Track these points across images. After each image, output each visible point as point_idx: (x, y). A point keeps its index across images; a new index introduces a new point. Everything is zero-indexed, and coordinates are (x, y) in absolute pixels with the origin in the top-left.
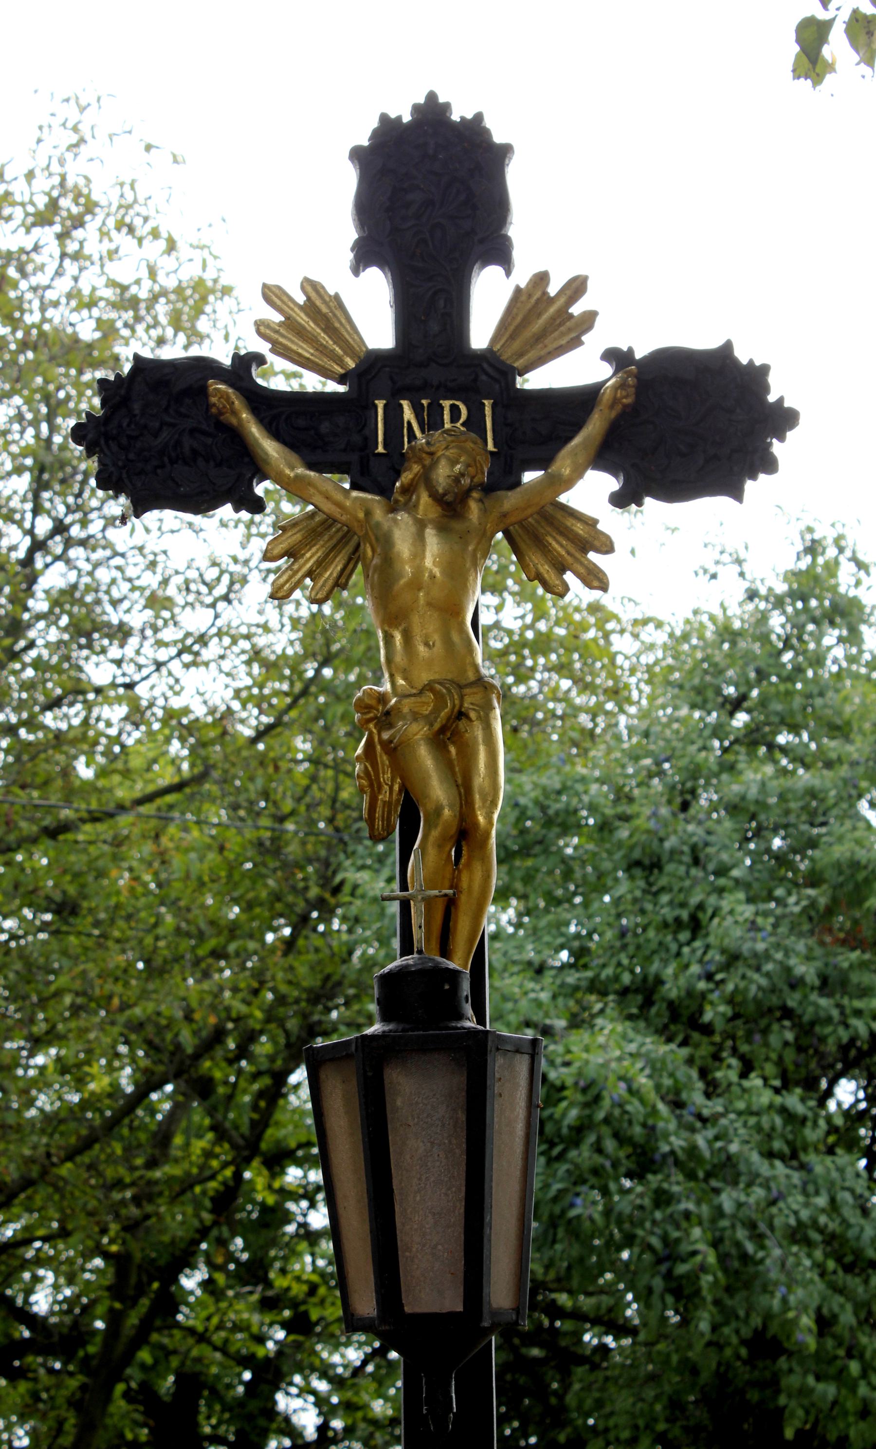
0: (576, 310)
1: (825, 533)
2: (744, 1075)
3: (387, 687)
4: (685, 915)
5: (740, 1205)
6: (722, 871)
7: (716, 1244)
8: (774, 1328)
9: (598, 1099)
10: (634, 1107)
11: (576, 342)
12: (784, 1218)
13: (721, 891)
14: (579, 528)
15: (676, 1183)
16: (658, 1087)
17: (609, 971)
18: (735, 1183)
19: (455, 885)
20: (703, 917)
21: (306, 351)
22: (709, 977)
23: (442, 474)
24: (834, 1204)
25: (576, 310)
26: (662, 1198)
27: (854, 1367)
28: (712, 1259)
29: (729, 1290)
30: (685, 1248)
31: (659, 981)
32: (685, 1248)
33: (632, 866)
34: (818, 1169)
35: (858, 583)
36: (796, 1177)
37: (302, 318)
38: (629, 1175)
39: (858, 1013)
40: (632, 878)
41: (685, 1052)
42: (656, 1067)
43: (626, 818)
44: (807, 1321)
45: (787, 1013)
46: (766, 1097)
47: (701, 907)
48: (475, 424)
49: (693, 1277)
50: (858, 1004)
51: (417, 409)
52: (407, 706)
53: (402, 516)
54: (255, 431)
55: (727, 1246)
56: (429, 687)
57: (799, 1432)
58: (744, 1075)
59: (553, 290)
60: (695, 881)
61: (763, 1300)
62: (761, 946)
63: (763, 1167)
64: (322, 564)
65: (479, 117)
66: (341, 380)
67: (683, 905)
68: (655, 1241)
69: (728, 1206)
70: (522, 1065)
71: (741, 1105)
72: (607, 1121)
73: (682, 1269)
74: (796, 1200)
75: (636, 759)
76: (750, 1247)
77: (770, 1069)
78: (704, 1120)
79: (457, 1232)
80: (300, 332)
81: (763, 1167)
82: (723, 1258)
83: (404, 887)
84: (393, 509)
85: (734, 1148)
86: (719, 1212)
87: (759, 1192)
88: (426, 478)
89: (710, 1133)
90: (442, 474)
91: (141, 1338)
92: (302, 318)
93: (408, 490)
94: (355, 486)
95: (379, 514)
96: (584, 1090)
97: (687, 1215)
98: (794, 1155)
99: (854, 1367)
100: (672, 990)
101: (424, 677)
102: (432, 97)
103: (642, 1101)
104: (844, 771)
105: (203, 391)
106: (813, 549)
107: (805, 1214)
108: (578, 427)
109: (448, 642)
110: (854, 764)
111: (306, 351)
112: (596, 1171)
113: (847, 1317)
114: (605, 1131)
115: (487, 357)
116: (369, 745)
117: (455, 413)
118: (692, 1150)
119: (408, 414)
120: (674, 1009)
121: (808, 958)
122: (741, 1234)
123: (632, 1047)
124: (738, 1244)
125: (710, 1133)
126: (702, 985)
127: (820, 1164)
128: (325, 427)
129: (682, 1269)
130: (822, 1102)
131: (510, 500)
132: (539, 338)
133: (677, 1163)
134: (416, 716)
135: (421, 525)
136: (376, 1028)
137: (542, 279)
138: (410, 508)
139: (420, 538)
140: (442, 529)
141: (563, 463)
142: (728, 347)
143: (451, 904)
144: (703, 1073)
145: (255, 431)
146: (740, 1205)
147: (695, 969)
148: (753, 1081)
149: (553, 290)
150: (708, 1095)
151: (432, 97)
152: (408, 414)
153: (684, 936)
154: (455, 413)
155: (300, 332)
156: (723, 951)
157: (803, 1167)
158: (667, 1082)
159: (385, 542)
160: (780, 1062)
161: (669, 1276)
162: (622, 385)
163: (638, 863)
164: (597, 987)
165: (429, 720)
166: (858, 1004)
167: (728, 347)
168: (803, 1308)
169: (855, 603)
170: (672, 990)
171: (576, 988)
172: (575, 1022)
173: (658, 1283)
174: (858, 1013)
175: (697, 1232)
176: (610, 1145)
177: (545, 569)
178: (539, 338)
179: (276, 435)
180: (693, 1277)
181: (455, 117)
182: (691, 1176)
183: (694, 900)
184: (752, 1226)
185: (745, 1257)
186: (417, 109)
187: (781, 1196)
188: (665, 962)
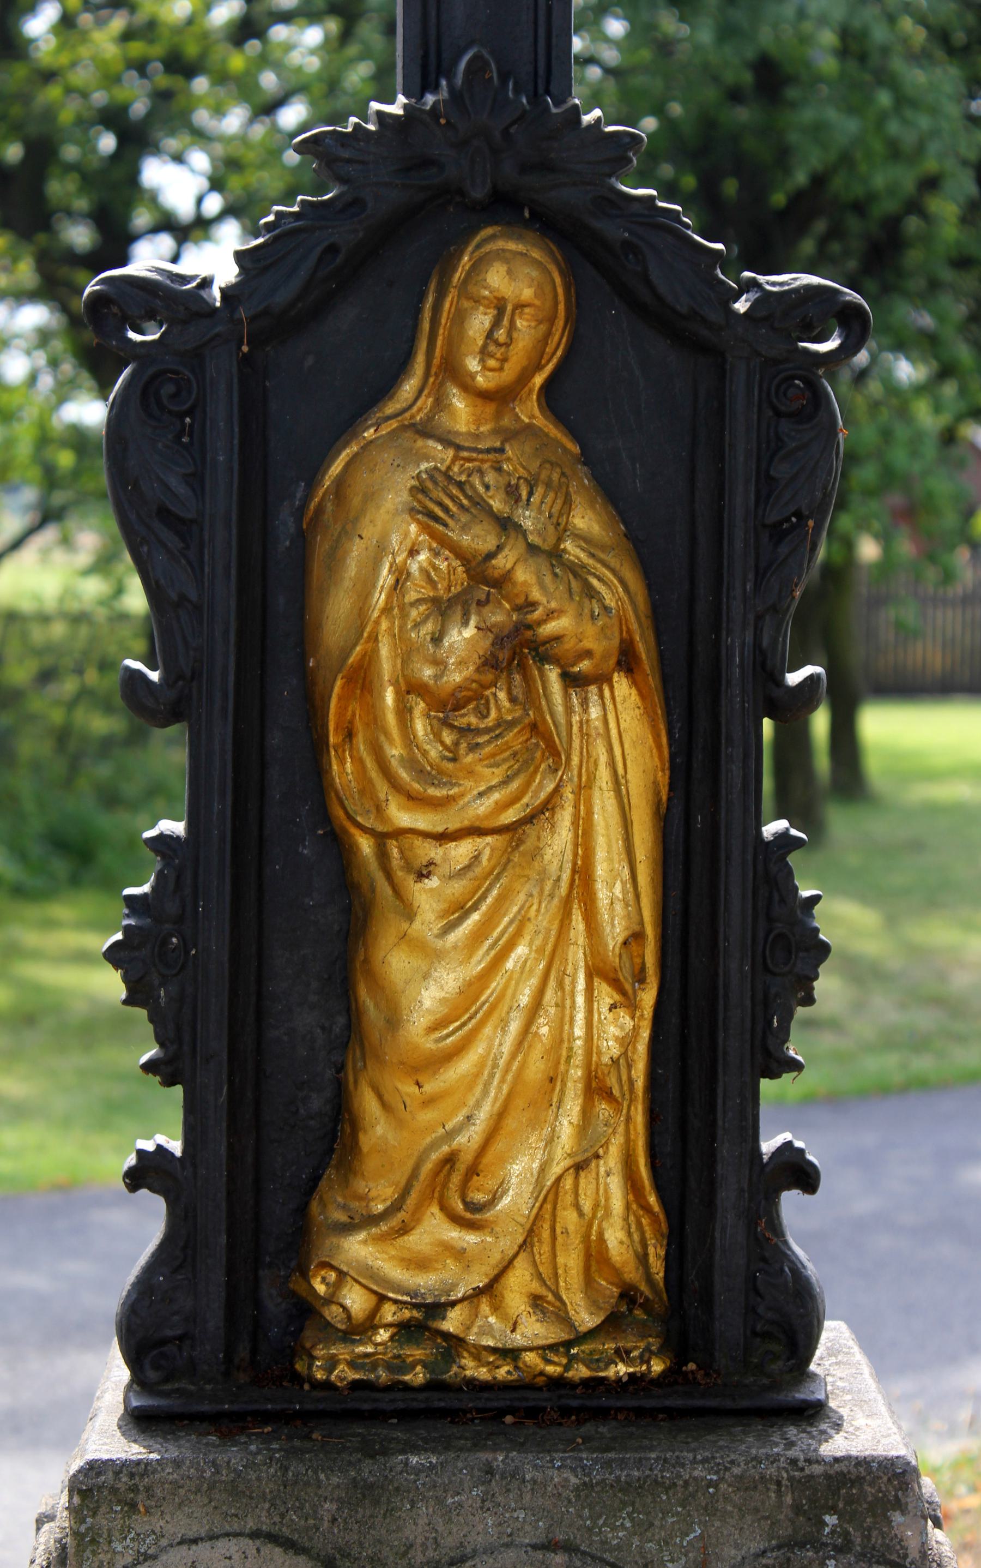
44: (828, 38)
99: (884, 98)
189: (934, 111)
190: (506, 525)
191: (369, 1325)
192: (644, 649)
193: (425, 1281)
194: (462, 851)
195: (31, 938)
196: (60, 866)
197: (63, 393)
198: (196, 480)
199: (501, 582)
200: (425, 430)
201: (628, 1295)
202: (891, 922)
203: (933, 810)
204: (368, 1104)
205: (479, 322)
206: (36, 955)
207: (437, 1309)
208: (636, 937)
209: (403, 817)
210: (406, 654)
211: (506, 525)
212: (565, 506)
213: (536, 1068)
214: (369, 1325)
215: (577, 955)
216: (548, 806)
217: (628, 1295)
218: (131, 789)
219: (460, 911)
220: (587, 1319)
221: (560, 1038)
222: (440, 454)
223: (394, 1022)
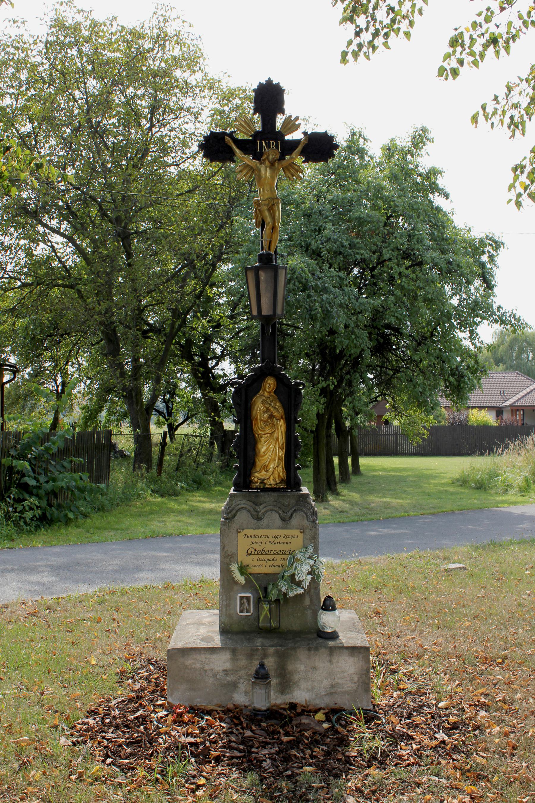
0: (297, 123)
1: (356, 130)
2: (330, 268)
3: (259, 199)
4: (317, 228)
5: (327, 298)
6: (327, 217)
7: (321, 307)
8: (334, 328)
9: (295, 272)
10: (303, 275)
11: (297, 129)
12: (338, 301)
13: (326, 222)
14: (296, 167)
15: (312, 293)
16: (309, 270)
17: (299, 242)
18: (326, 293)
19: (271, 237)
20: (322, 229)
21: (244, 130)
22: (322, 244)
23: (271, 157)
24: (349, 299)
25: (297, 123)
26: (309, 296)
27: (353, 336)
28: (320, 311)
29: (324, 318)
30: (314, 308)
31: (310, 244)
32: (314, 308)
33: (305, 215)
34: (346, 290)
35: (364, 144)
36: (341, 292)
37: (243, 123)
38: (301, 291)
39: (358, 253)
40: (304, 218)
41: (316, 262)
42: (308, 265)
43: (303, 203)
44: (342, 326)
45: (340, 253)
46: (335, 274)
47: (321, 226)
48: (277, 146)
49: (316, 315)
50: (358, 251)
51: (266, 143)
52: (263, 203)
53: (263, 165)
54: (234, 147)
55: (324, 308)
56: (267, 199)
57: (340, 351)
58: (330, 268)
59: (292, 119)
60: (320, 220)
61: (332, 321)
62: (336, 237)
63: (333, 290)
64: (247, 173)
65: (279, 83)
66: (251, 136)
67: (317, 226)
68: (307, 306)
69: (324, 299)
70: (284, 271)
71: (329, 275)
72: (296, 278)
73: (313, 313)
74: (340, 298)
75: (306, 188)
76: (329, 309)
77: (336, 266)
78: (320, 278)
79: (272, 301)
80: (243, 126)
81: (333, 290)
82: (323, 311)
83: (262, 238)
84: (261, 164)
85: (326, 285)
86: (322, 300)
87: (332, 296)
88: (267, 158)
89: (321, 281)
90: (271, 157)
91: (179, 330)
92: (243, 123)
93: (264, 160)
94: (253, 159)
95: (258, 165)
96: (291, 270)
97: (315, 300)
98: (341, 287)
99: (353, 336)
100: (313, 247)
101: (266, 197)
102: (269, 78)
103: (305, 274)
104: (359, 193)
105: (224, 139)
106: (353, 134)
107: (342, 301)
108: (297, 147)
109: (271, 190)
110: (361, 192)
111: (244, 130)
112: (293, 290)
113: (352, 325)
114: (296, 280)
115: (279, 132)
116: (256, 210)
117: (273, 144)
118: (317, 285)
119: (264, 144)
120: (314, 252)
121: (347, 240)
122: (327, 305)
123: (303, 260)
124: (326, 308)
125: (321, 281)
126: (321, 246)
127: (347, 289)
128: (248, 146)
129: (313, 313)
130: (349, 274)
131: (284, 163)
132: (289, 129)
133: (313, 288)
134: (265, 205)
135: (266, 167)
136: (257, 264)
137: (290, 116)
138: (264, 164)
139: (266, 171)
140: (270, 168)
141: (294, 155)
142: (326, 132)
143: (270, 242)
144: (320, 267)
145: (234, 147)
146: (327, 298)
147: (319, 242)
148: (332, 270)
149: (292, 119)
150: (321, 272)
151: (269, 78)
152: (264, 144)
153: (317, 233)
154: (273, 144)
155: (243, 126)
156: (326, 237)
157: (343, 290)
158: (311, 269)
159: (259, 171)
160: (339, 264)
161: (310, 315)
162: (305, 140)
163: (306, 215)
164: (295, 246)
165: (268, 205)
166: (358, 251)
167: (326, 132)
168: (341, 322)
169: (364, 149)
170: (313, 247)
171: (290, 246)
172: (289, 254)
173: (307, 316)
174: (358, 253)
175: (317, 304)
176: (297, 284)
177: (290, 175)
178: (289, 129)
179: (238, 147)
180: (316, 315)
181: (274, 83)
182: (316, 291)
183: (320, 224)
184: (330, 303)
185: (328, 311)
186: (266, 81)
187: (337, 297)
188: (312, 240)
189: (362, 339)
190: (270, 404)
191: (257, 482)
192: (284, 416)
193: (263, 477)
194: (266, 436)
195: (191, 498)
196: (195, 486)
197: (194, 391)
198: (241, 401)
199: (270, 410)
200: (262, 395)
201: (282, 480)
202: (361, 496)
203: (374, 476)
204: (257, 460)
205: (268, 385)
206: (192, 501)
207: (263, 480)
208: (283, 444)
209: (260, 432)
210: (261, 417)
211: (270, 404)
212: (340, 438)
213: (273, 457)
214: (257, 482)
215: (277, 446)
216: (274, 431)
217: (282, 480)
218: (208, 471)
219: (266, 441)
220: (278, 482)
221: (276, 454)
222: (264, 398)
223: (259, 452)
